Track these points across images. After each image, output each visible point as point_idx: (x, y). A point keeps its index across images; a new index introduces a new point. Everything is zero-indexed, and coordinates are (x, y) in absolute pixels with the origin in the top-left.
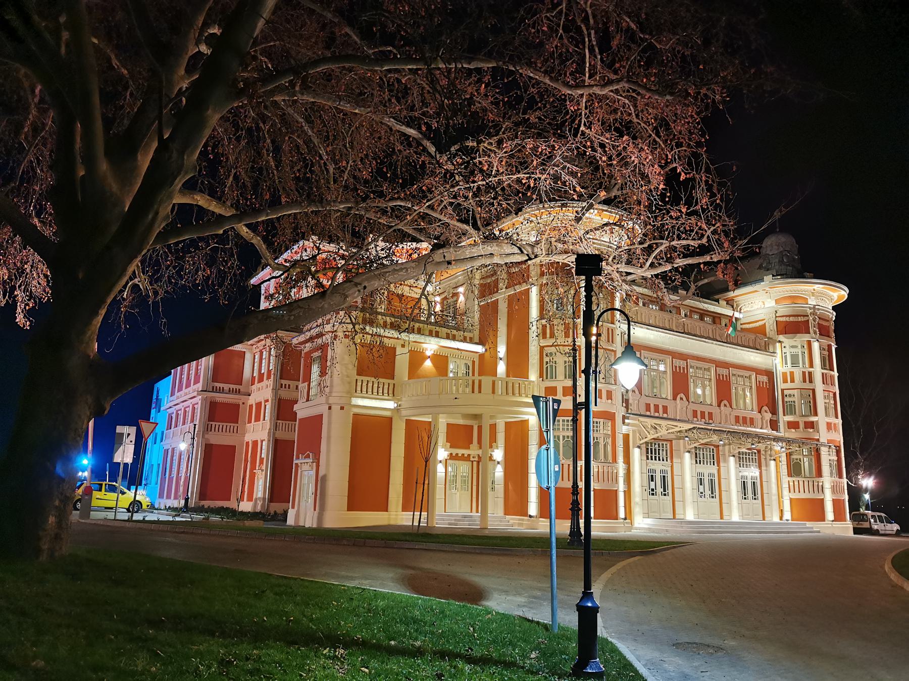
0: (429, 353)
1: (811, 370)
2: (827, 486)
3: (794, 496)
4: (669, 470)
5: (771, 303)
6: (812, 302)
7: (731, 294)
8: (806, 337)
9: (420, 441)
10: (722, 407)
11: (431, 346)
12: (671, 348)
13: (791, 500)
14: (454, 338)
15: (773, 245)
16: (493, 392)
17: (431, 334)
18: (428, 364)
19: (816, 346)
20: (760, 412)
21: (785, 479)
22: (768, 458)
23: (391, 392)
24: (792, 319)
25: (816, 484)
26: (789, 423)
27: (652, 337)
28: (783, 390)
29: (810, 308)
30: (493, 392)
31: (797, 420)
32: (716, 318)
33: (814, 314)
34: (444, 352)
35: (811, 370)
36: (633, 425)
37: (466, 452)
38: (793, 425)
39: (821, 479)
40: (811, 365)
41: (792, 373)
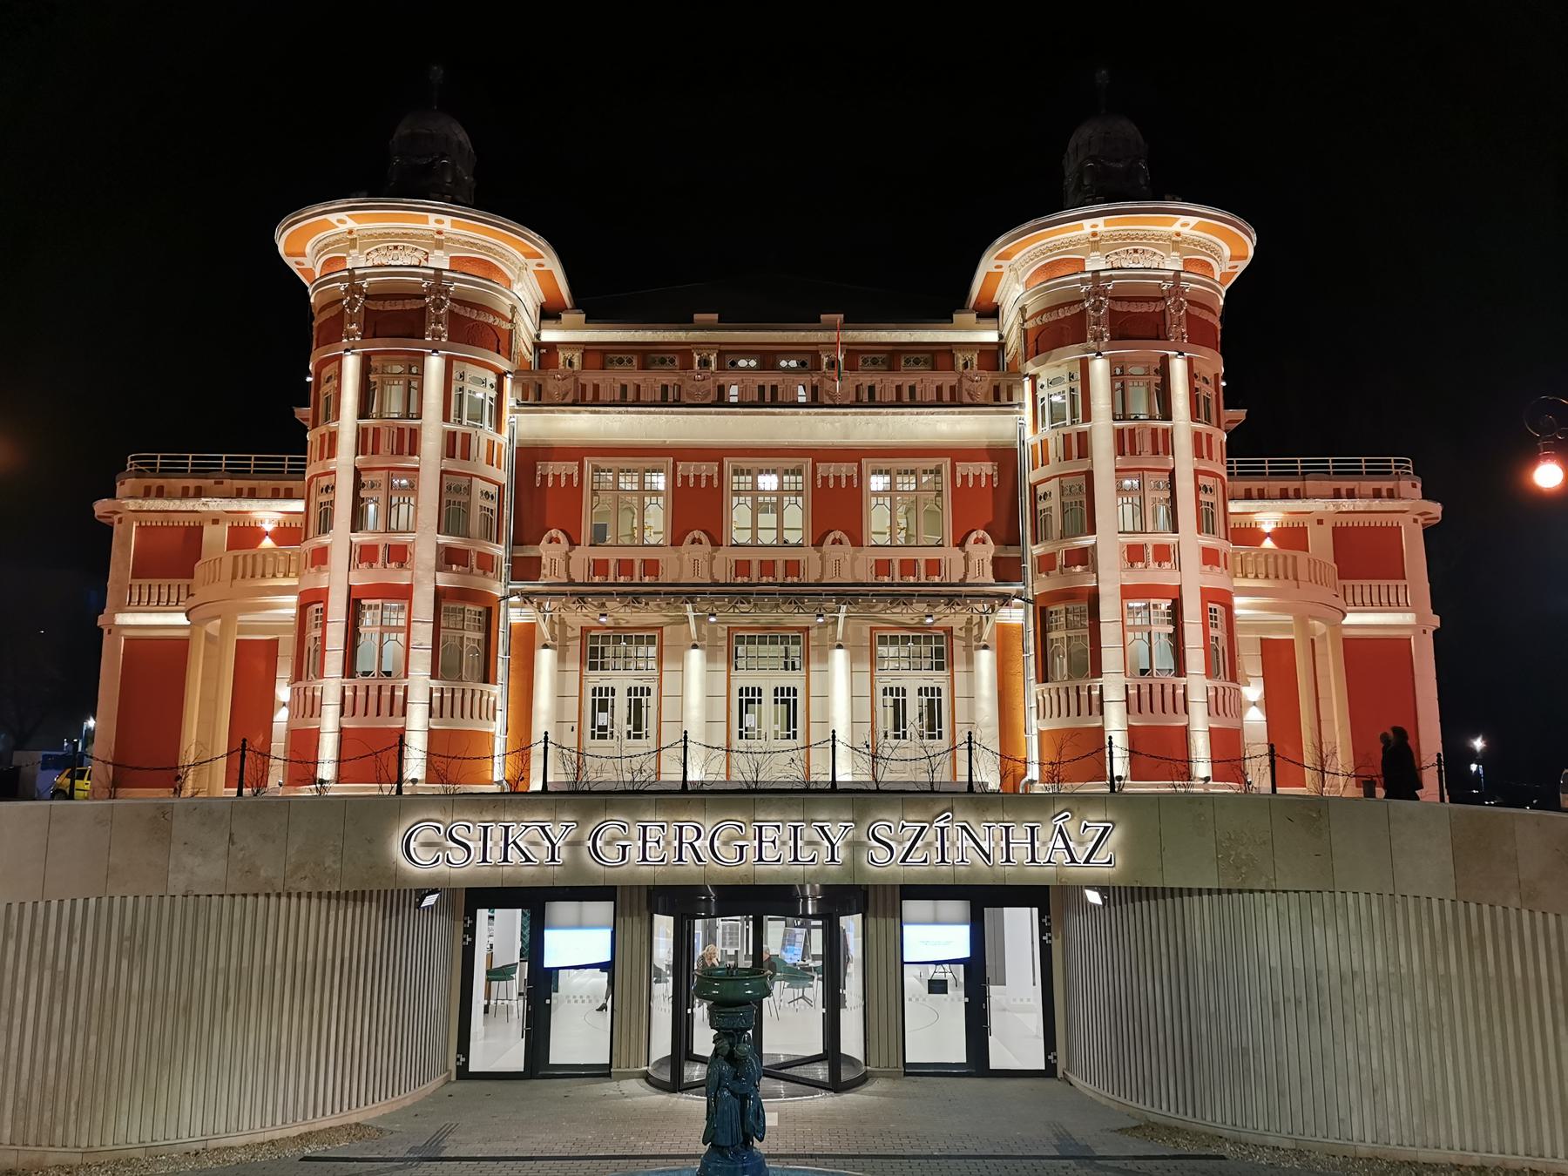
0: (268, 527)
1: (1167, 424)
2: (1197, 698)
3: (349, 723)
4: (654, 687)
6: (1096, 262)
8: (1073, 353)
12: (669, 441)
13: (1040, 733)
14: (160, 493)
19: (1099, 367)
20: (961, 544)
21: (1032, 692)
25: (1084, 693)
28: (1034, 488)
32: (940, 356)
34: (1297, 521)
39: (1097, 682)
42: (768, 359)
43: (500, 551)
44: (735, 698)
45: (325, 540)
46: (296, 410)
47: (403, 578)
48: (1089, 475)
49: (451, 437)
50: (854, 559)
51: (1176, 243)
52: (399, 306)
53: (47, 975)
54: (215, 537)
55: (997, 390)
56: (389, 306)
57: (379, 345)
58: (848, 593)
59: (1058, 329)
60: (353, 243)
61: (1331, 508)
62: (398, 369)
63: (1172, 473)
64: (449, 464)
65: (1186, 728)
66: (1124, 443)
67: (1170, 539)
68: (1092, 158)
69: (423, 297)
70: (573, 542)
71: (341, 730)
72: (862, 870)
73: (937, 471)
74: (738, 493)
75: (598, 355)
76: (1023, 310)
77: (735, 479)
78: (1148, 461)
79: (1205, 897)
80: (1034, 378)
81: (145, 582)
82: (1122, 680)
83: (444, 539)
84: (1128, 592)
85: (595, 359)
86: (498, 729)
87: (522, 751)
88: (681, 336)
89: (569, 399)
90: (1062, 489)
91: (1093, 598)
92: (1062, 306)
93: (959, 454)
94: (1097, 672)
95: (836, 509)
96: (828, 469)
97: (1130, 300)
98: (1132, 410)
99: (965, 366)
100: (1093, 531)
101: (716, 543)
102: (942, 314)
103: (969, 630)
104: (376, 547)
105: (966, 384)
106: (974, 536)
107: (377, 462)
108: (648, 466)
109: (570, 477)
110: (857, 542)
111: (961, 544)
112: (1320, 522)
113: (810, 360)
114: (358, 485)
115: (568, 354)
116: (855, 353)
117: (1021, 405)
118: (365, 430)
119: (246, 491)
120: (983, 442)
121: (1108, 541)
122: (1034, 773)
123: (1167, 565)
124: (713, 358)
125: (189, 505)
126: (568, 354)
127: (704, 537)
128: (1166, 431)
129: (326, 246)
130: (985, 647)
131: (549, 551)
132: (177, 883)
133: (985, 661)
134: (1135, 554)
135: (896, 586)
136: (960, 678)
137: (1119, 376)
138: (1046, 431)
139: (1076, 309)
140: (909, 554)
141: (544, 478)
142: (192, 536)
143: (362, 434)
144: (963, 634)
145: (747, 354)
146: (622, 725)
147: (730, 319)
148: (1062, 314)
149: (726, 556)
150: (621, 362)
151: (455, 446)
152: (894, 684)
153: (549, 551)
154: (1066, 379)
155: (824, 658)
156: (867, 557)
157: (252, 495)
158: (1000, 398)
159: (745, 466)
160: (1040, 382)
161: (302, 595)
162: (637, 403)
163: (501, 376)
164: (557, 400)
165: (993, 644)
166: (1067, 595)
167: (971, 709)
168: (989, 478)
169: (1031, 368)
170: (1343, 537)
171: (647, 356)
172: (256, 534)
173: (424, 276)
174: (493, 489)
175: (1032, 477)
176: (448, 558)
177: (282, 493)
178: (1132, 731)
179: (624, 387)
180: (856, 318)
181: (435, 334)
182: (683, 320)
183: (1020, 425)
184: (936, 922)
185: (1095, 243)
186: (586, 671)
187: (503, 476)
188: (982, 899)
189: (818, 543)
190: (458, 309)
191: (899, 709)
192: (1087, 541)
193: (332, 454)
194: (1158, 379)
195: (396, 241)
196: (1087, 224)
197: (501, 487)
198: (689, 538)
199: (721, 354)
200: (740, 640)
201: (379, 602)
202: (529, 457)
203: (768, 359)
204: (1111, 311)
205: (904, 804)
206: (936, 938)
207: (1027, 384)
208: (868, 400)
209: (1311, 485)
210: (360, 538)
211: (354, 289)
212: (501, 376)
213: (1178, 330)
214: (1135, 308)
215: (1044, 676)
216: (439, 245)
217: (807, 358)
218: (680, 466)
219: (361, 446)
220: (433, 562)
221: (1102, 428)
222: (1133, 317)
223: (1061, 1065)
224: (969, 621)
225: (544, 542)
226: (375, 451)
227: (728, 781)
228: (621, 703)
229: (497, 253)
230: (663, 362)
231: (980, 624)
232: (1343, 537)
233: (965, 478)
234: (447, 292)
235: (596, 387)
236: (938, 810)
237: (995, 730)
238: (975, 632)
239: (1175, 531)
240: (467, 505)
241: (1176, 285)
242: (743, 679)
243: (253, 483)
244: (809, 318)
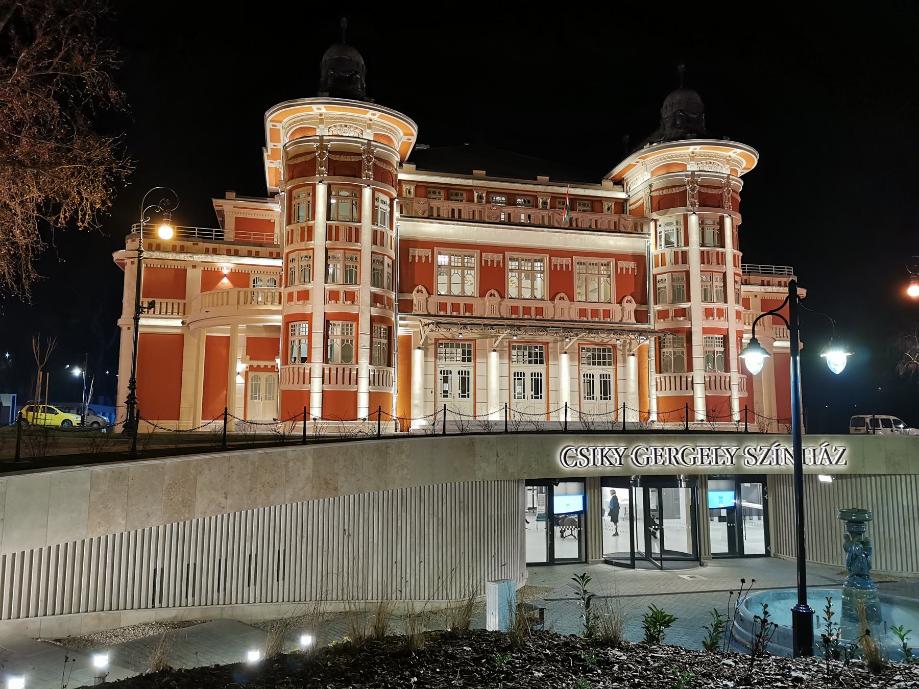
3: (327, 388)
4: (471, 371)
5: (648, 176)
6: (692, 167)
7: (617, 171)
8: (680, 211)
9: (217, 355)
10: (624, 304)
11: (226, 264)
12: (478, 241)
13: (658, 398)
14: (257, 255)
15: (673, 104)
16: (238, 303)
17: (229, 253)
18: (225, 281)
19: (693, 220)
20: (620, 303)
21: (653, 377)
22: (627, 353)
23: (181, 310)
24: (665, 192)
26: (659, 312)
27: (451, 231)
28: (655, 276)
29: (687, 176)
30: (238, 303)
31: (666, 308)
32: (595, 204)
33: (692, 182)
34: (244, 270)
35: (375, 227)
36: (412, 326)
37: (269, 364)
38: (662, 315)
39: (691, 374)
40: (687, 243)
41: (663, 255)
42: (511, 199)
43: (393, 295)
44: (512, 377)
45: (308, 287)
46: (214, 200)
47: (354, 310)
48: (688, 273)
49: (375, 233)
51: (728, 161)
52: (348, 159)
53: (435, 519)
54: (194, 277)
55: (636, 225)
56: (343, 158)
57: (338, 180)
58: (569, 328)
59: (669, 199)
60: (321, 121)
61: (763, 290)
62: (346, 194)
63: (725, 274)
64: (376, 249)
65: (730, 397)
66: (704, 258)
67: (723, 306)
68: (682, 111)
69: (360, 155)
71: (323, 391)
72: (742, 467)
73: (608, 265)
74: (512, 270)
75: (424, 189)
76: (651, 186)
77: (510, 263)
78: (715, 267)
79: (858, 479)
80: (656, 221)
82: (703, 373)
83: (374, 289)
84: (705, 331)
85: (422, 191)
88: (470, 182)
89: (426, 215)
90: (673, 280)
91: (689, 333)
92: (675, 187)
93: (619, 257)
94: (690, 369)
95: (561, 282)
96: (557, 261)
97: (708, 187)
98: (706, 242)
99: (608, 209)
100: (689, 300)
102: (596, 179)
103: (624, 346)
104: (338, 292)
105: (622, 221)
106: (626, 298)
107: (338, 245)
108: (466, 254)
109: (427, 258)
110: (571, 299)
111: (620, 303)
112: (756, 296)
113: (531, 201)
114: (327, 258)
115: (408, 187)
116: (557, 199)
117: (649, 234)
118: (330, 227)
119: (211, 250)
120: (630, 251)
121: (696, 305)
122: (654, 417)
123: (722, 319)
124: (484, 195)
125: (182, 256)
126: (408, 187)
127: (496, 294)
128: (722, 253)
129: (302, 120)
130: (633, 355)
131: (417, 297)
132: (479, 476)
133: (632, 361)
134: (708, 313)
135: (589, 323)
136: (620, 370)
137: (702, 223)
138: (663, 249)
139: (682, 189)
141: (414, 257)
142: (180, 275)
143: (329, 229)
144: (621, 348)
145: (500, 194)
146: (529, 392)
147: (493, 174)
148: (674, 191)
149: (577, 306)
150: (434, 193)
151: (377, 238)
152: (589, 372)
153: (417, 297)
154: (675, 223)
155: (556, 358)
157: (215, 252)
158: (637, 229)
159: (515, 257)
160: (658, 223)
161: (285, 317)
162: (460, 219)
163: (392, 200)
164: (420, 215)
165: (636, 354)
166: (675, 331)
167: (625, 386)
168: (633, 270)
169: (655, 216)
171: (451, 192)
172: (218, 276)
173: (362, 144)
175: (654, 271)
177: (275, 255)
179: (453, 210)
180: (557, 178)
181: (367, 176)
182: (466, 172)
183: (650, 244)
184: (566, 494)
185: (693, 157)
188: (738, 480)
189: (552, 299)
190: (378, 163)
191: (591, 384)
192: (686, 305)
193: (310, 238)
194: (718, 227)
195: (346, 122)
196: (692, 148)
198: (488, 293)
199: (488, 193)
200: (514, 348)
201: (340, 322)
202: (406, 245)
203: (511, 199)
204: (699, 192)
205: (758, 438)
206: (720, 498)
207: (652, 224)
208: (573, 226)
210: (329, 287)
211: (322, 147)
212: (392, 200)
213: (728, 204)
214: (710, 191)
215: (659, 370)
216: (369, 127)
217: (531, 199)
218: (484, 255)
219: (329, 236)
220: (369, 302)
221: (694, 250)
222: (709, 197)
223: (773, 552)
224: (625, 342)
225: (415, 292)
226: (337, 239)
228: (455, 379)
229: (391, 130)
230: (457, 195)
231: (630, 343)
233: (622, 269)
234: (373, 153)
235: (460, 211)
236: (773, 441)
237: (637, 396)
238: (628, 347)
239: (726, 302)
240: (382, 271)
241: (728, 182)
242: (443, 365)
243: (216, 246)
244: (531, 177)
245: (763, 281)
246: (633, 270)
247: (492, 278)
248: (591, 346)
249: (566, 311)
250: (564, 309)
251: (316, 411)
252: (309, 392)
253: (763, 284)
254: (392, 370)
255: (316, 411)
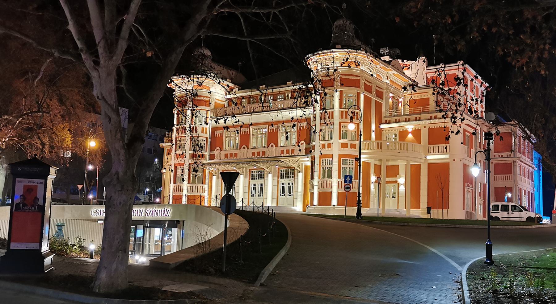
8: (356, 90)
34: (418, 127)
50: (276, 150)
70: (248, 148)
81: (432, 146)
86: (206, 195)
87: (210, 199)
101: (276, 146)
110: (276, 146)
112: (425, 127)
139: (359, 78)
140: (288, 148)
146: (258, 193)
149: (251, 151)
153: (216, 152)
156: (279, 150)
170: (431, 131)
174: (205, 139)
176: (193, 156)
178: (320, 193)
186: (280, 179)
187: (208, 135)
197: (207, 138)
209: (423, 116)
227: (146, 207)
232: (431, 131)
244: (284, 83)
245: (406, 119)
246: (306, 126)
247: (245, 140)
248: (285, 169)
249: (245, 154)
250: (274, 151)
251: (334, 202)
252: (331, 192)
253: (431, 118)
254: (204, 186)
255: (334, 202)
